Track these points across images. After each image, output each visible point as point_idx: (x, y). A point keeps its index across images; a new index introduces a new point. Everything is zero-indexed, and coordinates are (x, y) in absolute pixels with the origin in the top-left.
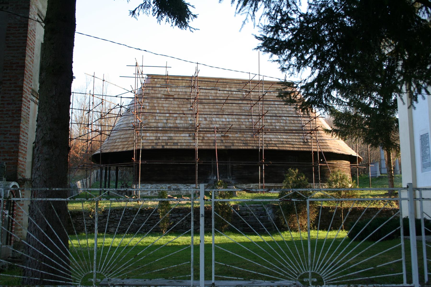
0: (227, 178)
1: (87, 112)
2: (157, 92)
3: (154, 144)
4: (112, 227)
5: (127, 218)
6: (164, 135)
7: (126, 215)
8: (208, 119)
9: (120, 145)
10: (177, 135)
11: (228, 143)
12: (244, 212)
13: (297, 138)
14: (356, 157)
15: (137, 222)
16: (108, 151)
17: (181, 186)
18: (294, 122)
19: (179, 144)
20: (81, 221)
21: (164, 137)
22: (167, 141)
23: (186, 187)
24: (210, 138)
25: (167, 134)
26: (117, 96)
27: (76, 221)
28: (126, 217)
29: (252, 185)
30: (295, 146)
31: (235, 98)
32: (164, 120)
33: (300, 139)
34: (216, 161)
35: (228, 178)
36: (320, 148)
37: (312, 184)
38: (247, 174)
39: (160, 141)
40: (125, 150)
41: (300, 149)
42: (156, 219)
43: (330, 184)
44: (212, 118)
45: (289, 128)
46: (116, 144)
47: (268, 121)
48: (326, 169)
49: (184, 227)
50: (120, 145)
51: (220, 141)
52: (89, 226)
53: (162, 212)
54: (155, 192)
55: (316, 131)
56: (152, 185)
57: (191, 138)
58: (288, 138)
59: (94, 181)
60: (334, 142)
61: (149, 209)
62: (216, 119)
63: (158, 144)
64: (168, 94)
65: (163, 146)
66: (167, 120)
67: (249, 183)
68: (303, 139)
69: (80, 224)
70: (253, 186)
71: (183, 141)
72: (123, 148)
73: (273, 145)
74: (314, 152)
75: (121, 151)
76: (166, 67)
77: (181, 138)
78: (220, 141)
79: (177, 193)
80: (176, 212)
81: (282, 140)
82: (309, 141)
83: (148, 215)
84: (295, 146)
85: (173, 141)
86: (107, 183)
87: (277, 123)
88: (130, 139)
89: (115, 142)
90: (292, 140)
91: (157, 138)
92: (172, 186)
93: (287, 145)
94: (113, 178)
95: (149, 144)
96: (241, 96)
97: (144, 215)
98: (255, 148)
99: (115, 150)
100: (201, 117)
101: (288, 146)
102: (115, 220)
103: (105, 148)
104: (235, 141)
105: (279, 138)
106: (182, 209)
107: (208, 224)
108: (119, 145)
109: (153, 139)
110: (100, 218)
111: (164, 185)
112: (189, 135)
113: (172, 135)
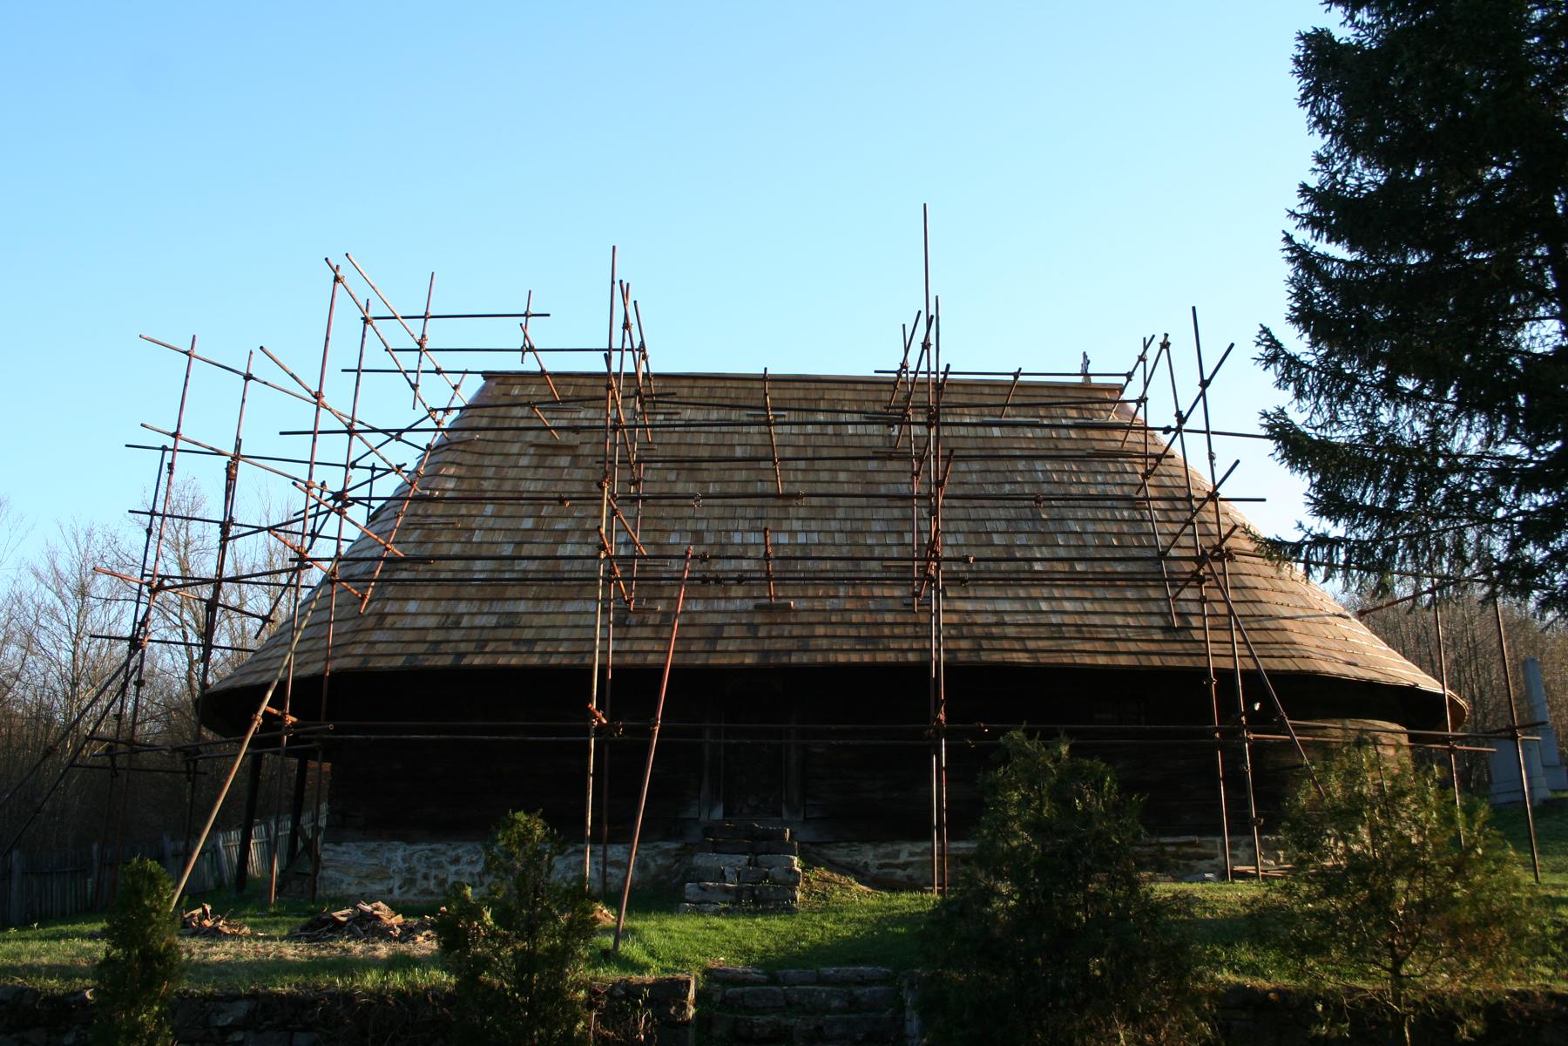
0: (781, 816)
8: (709, 538)
12: (762, 1020)
13: (1131, 608)
14: (1441, 697)
21: (476, 615)
24: (697, 616)
25: (500, 604)
29: (906, 851)
30: (1121, 646)
31: (852, 453)
33: (1151, 614)
36: (1252, 656)
37: (1219, 840)
39: (456, 635)
41: (1145, 661)
43: (1307, 839)
44: (728, 531)
45: (1097, 567)
47: (997, 539)
48: (1288, 760)
51: (812, 647)
54: (425, 884)
55: (1220, 559)
56: (411, 848)
58: (1086, 613)
60: (1321, 627)
64: (553, 442)
66: (519, 544)
67: (891, 840)
68: (1161, 614)
70: (912, 854)
73: (1006, 644)
74: (1219, 672)
77: (559, 620)
78: (743, 632)
81: (1055, 619)
82: (1195, 622)
84: (1121, 646)
85: (517, 634)
87: (1039, 546)
90: (1107, 620)
93: (1080, 646)
96: (879, 442)
98: (911, 657)
100: (680, 531)
101: (1088, 646)
111: (469, 846)
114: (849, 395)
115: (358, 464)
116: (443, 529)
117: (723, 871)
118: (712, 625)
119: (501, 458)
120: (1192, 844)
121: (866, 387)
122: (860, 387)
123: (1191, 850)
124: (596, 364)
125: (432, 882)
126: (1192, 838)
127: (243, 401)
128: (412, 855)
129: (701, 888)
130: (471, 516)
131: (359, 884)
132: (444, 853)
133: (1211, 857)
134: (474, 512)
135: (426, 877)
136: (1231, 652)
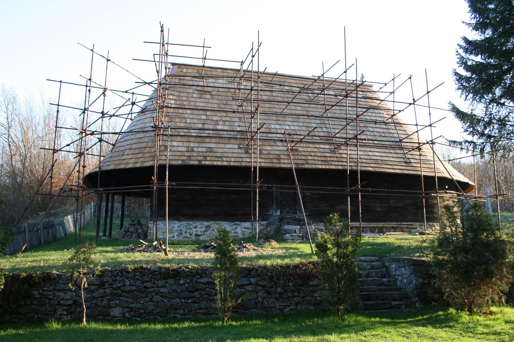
0: (296, 213)
3: (185, 158)
4: (117, 305)
5: (146, 287)
6: (200, 145)
7: (145, 282)
9: (131, 159)
10: (219, 146)
11: (299, 159)
15: (168, 295)
16: (110, 168)
17: (226, 225)
18: (384, 134)
19: (225, 159)
20: (51, 293)
22: (204, 154)
23: (234, 227)
26: (126, 92)
27: (42, 294)
28: (145, 284)
32: (199, 125)
34: (295, 183)
38: (326, 208)
39: (195, 154)
40: (138, 165)
42: (204, 290)
44: (269, 124)
46: (124, 157)
48: (435, 202)
49: (259, 305)
50: (131, 159)
52: (68, 305)
53: (220, 277)
54: (185, 235)
56: (180, 223)
57: (242, 151)
58: (382, 156)
59: (91, 217)
61: (191, 269)
62: (275, 125)
63: (192, 157)
65: (199, 161)
66: (203, 124)
69: (50, 299)
71: (230, 155)
72: (136, 163)
75: (133, 167)
76: (203, 47)
77: (227, 150)
78: (286, 157)
80: (243, 275)
83: (188, 281)
85: (215, 154)
86: (108, 220)
88: (147, 150)
89: (123, 155)
91: (190, 149)
92: (212, 225)
94: (118, 212)
95: (177, 158)
97: (182, 282)
99: (122, 167)
102: (123, 291)
103: (107, 164)
104: (310, 158)
105: (370, 155)
106: (254, 269)
107: (304, 297)
108: (129, 159)
109: (183, 150)
110: (93, 287)
111: (200, 222)
112: (239, 147)
113: (212, 145)
114: (293, 81)
115: (128, 92)
116: (175, 117)
117: (295, 231)
118: (276, 154)
119: (187, 94)
120: (411, 225)
121: (298, 79)
122: (296, 79)
123: (410, 226)
124: (237, 66)
125: (188, 234)
126: (411, 223)
127: (107, 68)
128: (181, 225)
129: (291, 235)
130: (184, 113)
131: (163, 235)
132: (192, 225)
133: (416, 228)
134: (184, 112)
135: (186, 232)
136: (434, 171)
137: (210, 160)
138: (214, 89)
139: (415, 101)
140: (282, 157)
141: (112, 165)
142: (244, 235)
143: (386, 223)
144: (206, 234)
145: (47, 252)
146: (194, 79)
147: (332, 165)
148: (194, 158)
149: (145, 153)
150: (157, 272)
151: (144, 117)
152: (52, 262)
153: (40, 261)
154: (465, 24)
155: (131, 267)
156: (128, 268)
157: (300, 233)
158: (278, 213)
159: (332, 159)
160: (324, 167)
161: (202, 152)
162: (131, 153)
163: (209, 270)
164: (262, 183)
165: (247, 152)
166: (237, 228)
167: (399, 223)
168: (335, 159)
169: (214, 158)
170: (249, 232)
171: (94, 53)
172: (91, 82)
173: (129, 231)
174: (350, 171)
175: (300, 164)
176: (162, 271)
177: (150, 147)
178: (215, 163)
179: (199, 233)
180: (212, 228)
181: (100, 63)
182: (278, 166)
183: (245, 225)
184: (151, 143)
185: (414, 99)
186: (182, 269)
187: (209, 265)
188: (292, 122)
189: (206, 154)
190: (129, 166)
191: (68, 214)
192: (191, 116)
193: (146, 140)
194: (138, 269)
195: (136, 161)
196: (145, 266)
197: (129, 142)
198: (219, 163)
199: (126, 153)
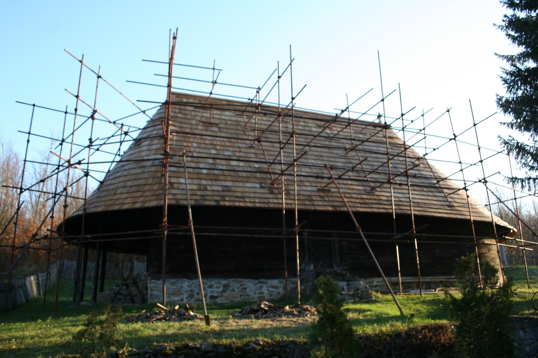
1: (58, 143)
2: (189, 117)
3: (198, 198)
6: (214, 183)
10: (237, 184)
16: (99, 209)
17: (249, 284)
19: (247, 200)
22: (221, 193)
23: (258, 285)
35: (336, 268)
40: (138, 206)
46: (116, 197)
56: (191, 282)
61: (263, 346)
65: (216, 201)
71: (252, 195)
72: (134, 203)
76: (214, 69)
77: (247, 190)
79: (242, 297)
85: (233, 194)
88: (147, 187)
89: (115, 194)
92: (232, 284)
99: (116, 208)
111: (217, 280)
112: (261, 186)
128: (192, 284)
137: (230, 201)
138: (221, 121)
139: (455, 136)
140: (314, 198)
141: (101, 206)
142: (271, 295)
143: (434, 277)
144: (224, 296)
145: (12, 324)
146: (197, 110)
147: (373, 208)
148: (209, 198)
149: (146, 191)
150: (212, 353)
151: (140, 150)
152: (31, 342)
153: (10, 340)
154: (498, 56)
155: (169, 346)
156: (166, 348)
157: (349, 291)
158: (312, 267)
159: (371, 201)
160: (365, 210)
161: (218, 191)
162: (125, 191)
163: (290, 346)
164: (302, 227)
165: (272, 193)
166: (262, 287)
167: (448, 277)
168: (374, 201)
169: (233, 199)
170: (277, 292)
171: (83, 66)
172: (79, 101)
173: (120, 294)
174: (397, 214)
175: (337, 206)
176: (220, 350)
177: (150, 184)
178: (237, 204)
179: (215, 294)
180: (231, 288)
181: (89, 78)
182: (312, 208)
183: (272, 283)
184: (151, 180)
185: (454, 135)
186: (250, 347)
187: (302, 339)
188: (316, 161)
189: (224, 194)
190: (126, 207)
191: (30, 275)
192: (198, 150)
193: (145, 175)
194: (182, 350)
195: (135, 200)
196: (191, 344)
197: (121, 179)
198: (242, 204)
199: (118, 192)
